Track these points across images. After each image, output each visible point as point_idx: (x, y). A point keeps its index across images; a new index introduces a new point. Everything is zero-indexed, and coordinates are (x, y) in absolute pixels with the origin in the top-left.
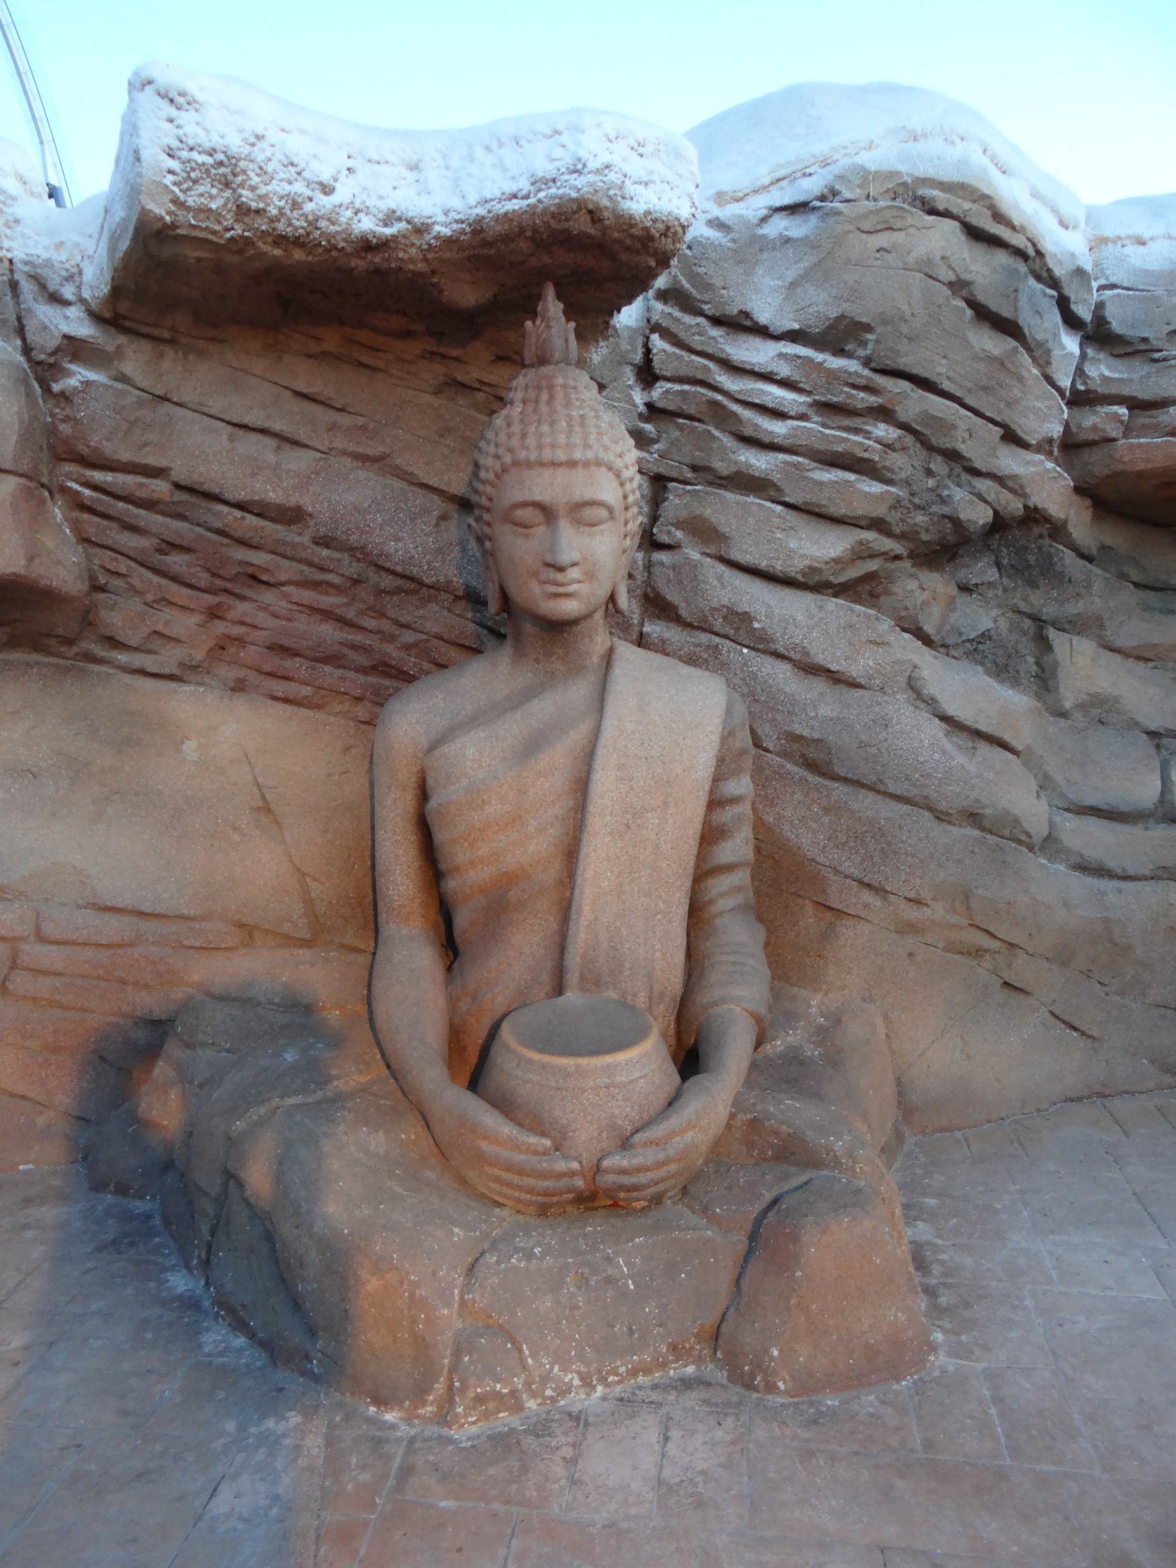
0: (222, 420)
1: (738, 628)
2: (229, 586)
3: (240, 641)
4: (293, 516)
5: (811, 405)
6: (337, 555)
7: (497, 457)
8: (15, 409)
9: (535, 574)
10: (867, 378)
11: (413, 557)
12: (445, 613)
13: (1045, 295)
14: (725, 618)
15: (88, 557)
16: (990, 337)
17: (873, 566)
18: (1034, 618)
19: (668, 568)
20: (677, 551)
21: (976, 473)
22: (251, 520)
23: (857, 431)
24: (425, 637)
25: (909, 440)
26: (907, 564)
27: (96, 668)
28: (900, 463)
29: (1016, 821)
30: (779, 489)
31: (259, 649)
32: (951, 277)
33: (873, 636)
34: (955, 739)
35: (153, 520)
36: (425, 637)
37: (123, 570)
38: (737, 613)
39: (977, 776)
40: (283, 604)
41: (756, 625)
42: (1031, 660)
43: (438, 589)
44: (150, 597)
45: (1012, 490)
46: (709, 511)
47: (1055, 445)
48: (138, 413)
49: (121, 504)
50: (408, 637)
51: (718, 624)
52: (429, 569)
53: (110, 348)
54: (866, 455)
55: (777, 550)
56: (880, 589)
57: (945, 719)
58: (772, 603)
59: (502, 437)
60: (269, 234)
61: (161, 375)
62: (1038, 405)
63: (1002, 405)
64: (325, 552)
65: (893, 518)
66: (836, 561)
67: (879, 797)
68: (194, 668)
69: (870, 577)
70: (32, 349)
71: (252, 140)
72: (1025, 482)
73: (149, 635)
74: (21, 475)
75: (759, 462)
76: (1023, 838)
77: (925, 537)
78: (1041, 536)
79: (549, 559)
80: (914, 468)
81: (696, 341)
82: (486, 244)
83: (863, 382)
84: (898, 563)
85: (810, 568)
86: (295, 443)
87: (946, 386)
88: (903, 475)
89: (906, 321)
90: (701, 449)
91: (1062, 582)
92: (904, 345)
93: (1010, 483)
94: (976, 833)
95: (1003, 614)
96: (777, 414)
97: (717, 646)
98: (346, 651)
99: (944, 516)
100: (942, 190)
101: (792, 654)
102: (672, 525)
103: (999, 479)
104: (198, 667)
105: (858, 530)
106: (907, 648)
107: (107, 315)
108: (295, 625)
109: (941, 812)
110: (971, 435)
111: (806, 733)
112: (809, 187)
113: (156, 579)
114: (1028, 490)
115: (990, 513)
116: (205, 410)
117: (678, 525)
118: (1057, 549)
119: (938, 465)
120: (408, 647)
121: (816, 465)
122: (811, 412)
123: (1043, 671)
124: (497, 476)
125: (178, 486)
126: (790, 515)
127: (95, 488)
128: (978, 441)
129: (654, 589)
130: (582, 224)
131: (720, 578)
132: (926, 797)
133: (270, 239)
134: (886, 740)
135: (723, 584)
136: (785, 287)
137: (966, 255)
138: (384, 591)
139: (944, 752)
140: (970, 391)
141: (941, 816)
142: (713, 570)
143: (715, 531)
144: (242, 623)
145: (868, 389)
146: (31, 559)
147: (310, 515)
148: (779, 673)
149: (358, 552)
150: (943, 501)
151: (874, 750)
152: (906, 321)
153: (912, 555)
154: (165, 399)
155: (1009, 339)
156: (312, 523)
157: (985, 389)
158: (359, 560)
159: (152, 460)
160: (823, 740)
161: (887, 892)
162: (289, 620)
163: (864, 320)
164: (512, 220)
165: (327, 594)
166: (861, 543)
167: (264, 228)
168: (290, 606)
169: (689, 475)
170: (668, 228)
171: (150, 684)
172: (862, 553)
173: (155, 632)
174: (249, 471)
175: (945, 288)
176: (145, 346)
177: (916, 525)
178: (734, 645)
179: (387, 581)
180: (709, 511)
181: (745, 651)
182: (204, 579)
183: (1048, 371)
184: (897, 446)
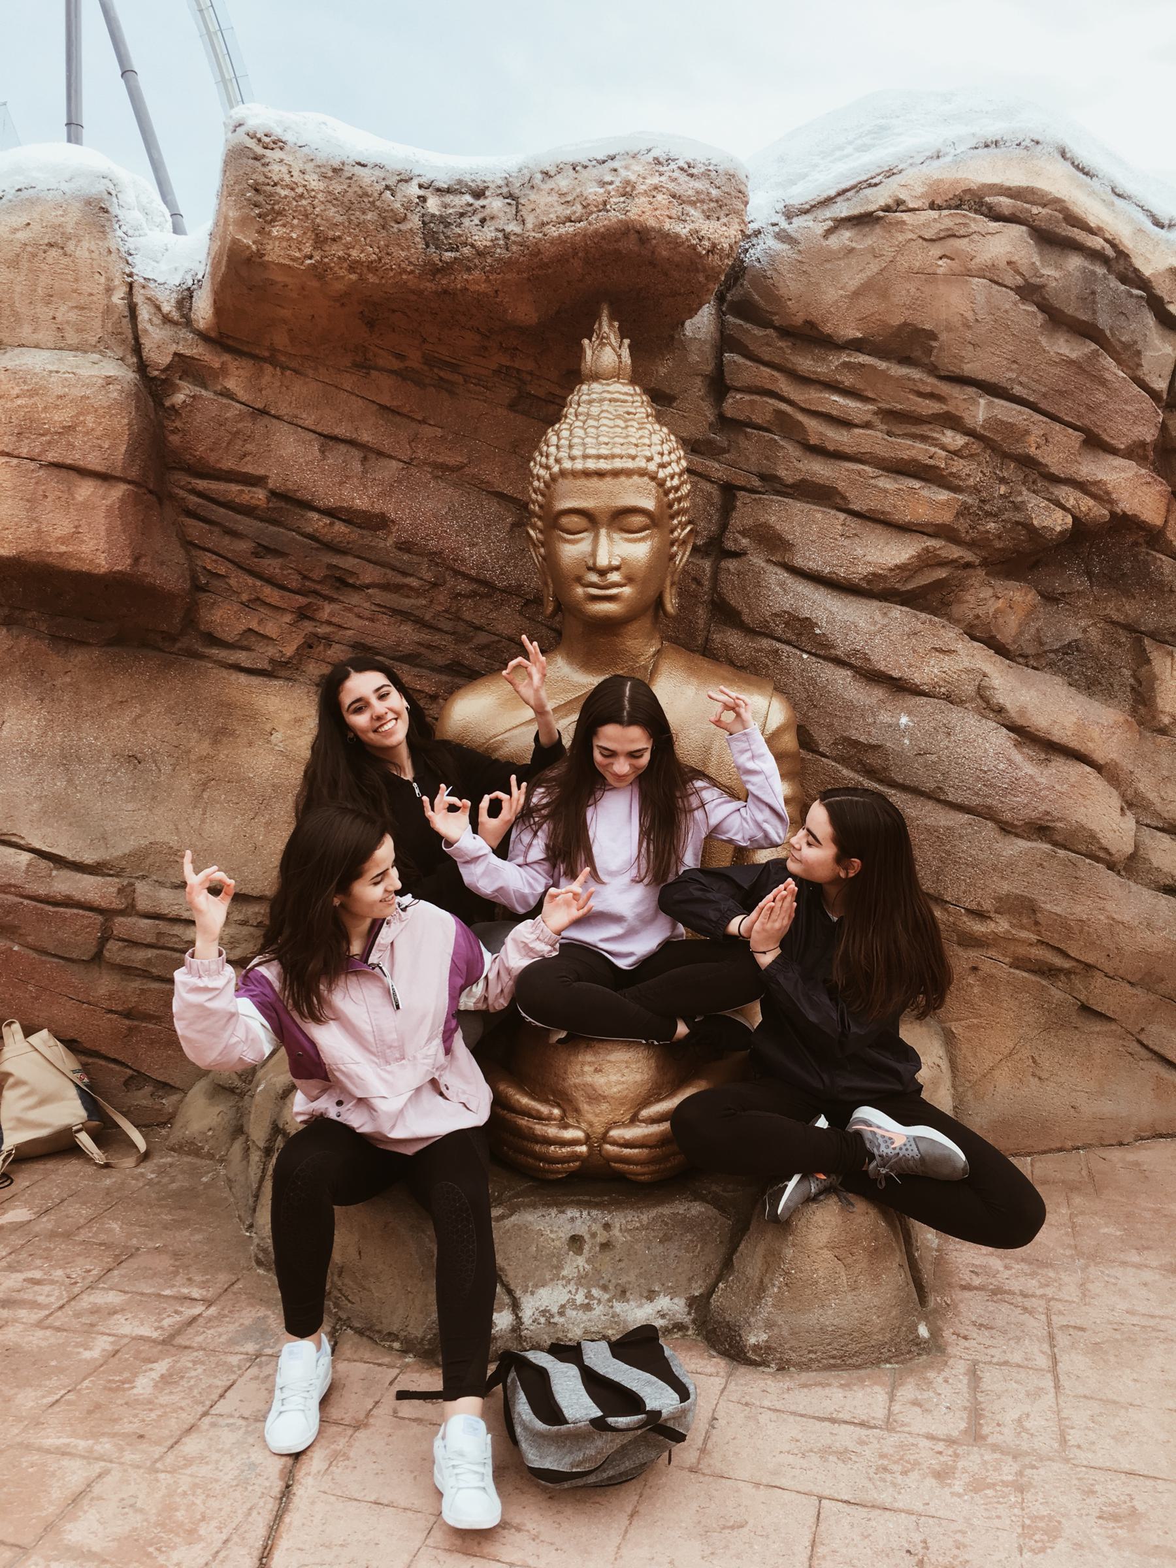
0: (315, 432)
1: (801, 634)
2: (318, 587)
3: (328, 641)
4: (377, 522)
5: (875, 413)
6: (416, 559)
7: (547, 467)
8: (126, 421)
9: (579, 580)
10: (933, 385)
11: (486, 562)
12: (517, 617)
13: (1131, 295)
14: (787, 624)
15: (190, 559)
16: (1067, 341)
17: (942, 573)
18: (1129, 628)
19: (733, 574)
20: (744, 558)
21: (1055, 480)
22: (340, 527)
23: (924, 438)
24: (497, 638)
25: (976, 447)
26: (981, 572)
27: (198, 663)
28: (966, 471)
29: (1093, 837)
30: (844, 498)
31: (343, 648)
32: (1019, 281)
33: (939, 644)
34: (1025, 750)
35: (243, 523)
36: (497, 638)
37: (222, 571)
38: (799, 619)
39: (1048, 788)
40: (367, 605)
41: (818, 631)
42: (1127, 672)
43: (510, 593)
44: (245, 597)
45: (1094, 496)
46: (773, 518)
47: (1150, 448)
48: (240, 425)
49: (222, 510)
50: (482, 638)
51: (779, 630)
52: (501, 574)
53: (217, 365)
54: (932, 462)
55: (839, 558)
56: (952, 597)
57: (1013, 728)
58: (834, 609)
59: (553, 450)
60: (345, 260)
61: (260, 390)
62: (1128, 408)
63: (1082, 410)
64: (406, 557)
65: (962, 525)
66: (901, 568)
67: (939, 807)
68: (285, 664)
69: (939, 584)
70: (147, 366)
71: (330, 174)
72: (1110, 487)
73: (245, 631)
74: (129, 482)
75: (820, 470)
76: (1102, 854)
77: (998, 545)
78: (1136, 544)
79: (590, 563)
80: (984, 474)
81: (766, 353)
82: (544, 266)
83: (929, 389)
84: (970, 571)
85: (874, 574)
86: (380, 454)
87: (1018, 390)
88: (971, 482)
89: (969, 327)
90: (767, 458)
91: (1163, 592)
92: (968, 353)
93: (1093, 489)
94: (1046, 847)
95: (1094, 624)
96: (845, 423)
97: (777, 651)
98: (422, 650)
99: (1018, 523)
100: (1010, 196)
101: (853, 661)
102: (739, 532)
103: (1082, 486)
104: (287, 663)
105: (925, 537)
106: (974, 659)
107: (213, 334)
108: (378, 625)
109: (1006, 823)
110: (1047, 440)
111: (862, 739)
112: (877, 199)
113: (250, 580)
114: (1114, 496)
115: (1069, 519)
116: (300, 422)
117: (744, 533)
118: (1155, 558)
119: (1010, 471)
120: (480, 649)
121: (878, 472)
122: (876, 421)
123: (1140, 683)
124: (547, 486)
125: (273, 494)
126: (854, 523)
127: (200, 494)
128: (1057, 449)
129: (719, 594)
130: (630, 244)
131: (782, 584)
132: (989, 807)
133: (345, 265)
134: (947, 748)
135: (785, 590)
136: (847, 297)
137: (1036, 259)
138: (459, 594)
139: (1010, 762)
140: (1044, 395)
141: (1007, 828)
142: (775, 577)
143: (779, 538)
144: (329, 623)
145: (932, 396)
146: (136, 560)
147: (393, 521)
148: (841, 680)
149: (435, 557)
150: (1018, 507)
151: (934, 758)
152: (969, 327)
153: (985, 563)
154: (264, 412)
155: (1088, 342)
156: (394, 529)
157: (1061, 393)
158: (437, 564)
159: (249, 469)
160: (880, 746)
161: (947, 902)
162: (372, 620)
163: (927, 327)
164: (565, 242)
165: (408, 597)
166: (927, 549)
167: (341, 253)
168: (373, 608)
169: (756, 483)
170: (714, 246)
171: (243, 678)
172: (927, 560)
173: (250, 630)
174: (338, 479)
175: (1012, 293)
176: (247, 363)
177: (988, 532)
178: (795, 651)
179: (463, 586)
180: (773, 518)
181: (805, 656)
182: (294, 582)
183: (1140, 373)
184: (966, 452)
